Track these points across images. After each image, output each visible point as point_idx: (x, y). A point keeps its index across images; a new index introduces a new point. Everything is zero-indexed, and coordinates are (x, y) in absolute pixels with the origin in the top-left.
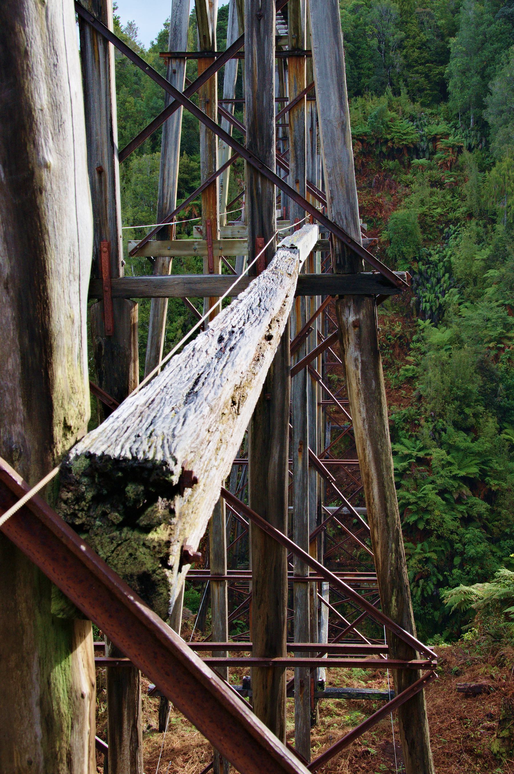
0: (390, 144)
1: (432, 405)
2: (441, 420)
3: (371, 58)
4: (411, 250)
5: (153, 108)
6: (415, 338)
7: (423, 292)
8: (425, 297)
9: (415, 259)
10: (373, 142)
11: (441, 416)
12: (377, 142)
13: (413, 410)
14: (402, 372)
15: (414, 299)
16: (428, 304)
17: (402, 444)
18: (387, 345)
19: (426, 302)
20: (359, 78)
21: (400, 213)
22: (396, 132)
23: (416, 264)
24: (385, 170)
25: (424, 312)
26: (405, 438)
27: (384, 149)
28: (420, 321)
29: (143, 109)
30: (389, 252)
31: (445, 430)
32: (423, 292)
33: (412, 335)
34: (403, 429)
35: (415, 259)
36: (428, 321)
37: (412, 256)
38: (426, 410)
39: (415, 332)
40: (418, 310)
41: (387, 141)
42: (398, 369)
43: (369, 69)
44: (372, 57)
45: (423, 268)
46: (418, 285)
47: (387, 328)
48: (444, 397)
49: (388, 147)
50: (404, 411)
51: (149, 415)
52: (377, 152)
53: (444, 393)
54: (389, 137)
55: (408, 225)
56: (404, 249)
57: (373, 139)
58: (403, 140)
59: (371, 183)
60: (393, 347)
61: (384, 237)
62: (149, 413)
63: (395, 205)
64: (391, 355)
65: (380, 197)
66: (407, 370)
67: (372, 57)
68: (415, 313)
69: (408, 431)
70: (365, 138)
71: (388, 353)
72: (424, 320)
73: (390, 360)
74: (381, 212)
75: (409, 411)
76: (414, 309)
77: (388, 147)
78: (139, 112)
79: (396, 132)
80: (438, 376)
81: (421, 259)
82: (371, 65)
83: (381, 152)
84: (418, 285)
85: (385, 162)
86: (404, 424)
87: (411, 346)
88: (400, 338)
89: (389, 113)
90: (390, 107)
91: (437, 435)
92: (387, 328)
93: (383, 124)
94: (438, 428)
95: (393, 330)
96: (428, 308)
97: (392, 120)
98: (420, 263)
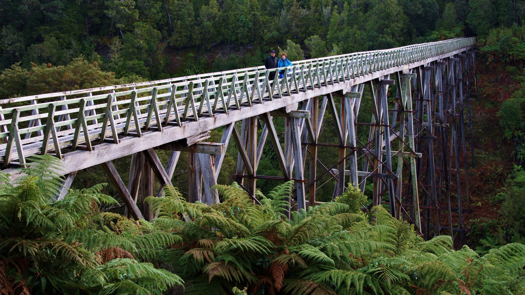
0: (511, 57)
1: (506, 220)
2: (512, 229)
3: (506, 5)
4: (514, 124)
5: (370, 36)
6: (509, 176)
7: (520, 148)
8: (520, 152)
9: (516, 129)
10: (501, 56)
11: (512, 227)
12: (504, 55)
13: (496, 221)
14: (497, 196)
15: (513, 152)
16: (522, 156)
17: (487, 240)
18: (492, 179)
19: (521, 154)
20: (498, 16)
21: (509, 101)
22: (516, 51)
23: (517, 131)
24: (507, 72)
25: (519, 160)
26: (489, 237)
27: (508, 60)
28: (515, 166)
29: (365, 37)
30: (501, 123)
31: (513, 235)
32: (520, 148)
33: (508, 174)
34: (488, 231)
35: (516, 129)
36: (520, 166)
37: (515, 127)
38: (503, 222)
39: (510, 173)
40: (516, 158)
41: (509, 55)
42: (496, 194)
43: (505, 11)
44: (507, 4)
45: (521, 134)
46: (517, 144)
47: (493, 169)
48: (514, 217)
49: (510, 59)
50: (490, 221)
51: (313, 62)
52: (503, 61)
53: (514, 214)
54: (511, 53)
55: (512, 109)
56: (509, 123)
57: (501, 54)
58: (520, 55)
59: (497, 79)
60: (495, 180)
61: (498, 114)
62: (312, 63)
63: (509, 95)
64: (493, 185)
65: (501, 89)
66: (501, 196)
67: (507, 4)
68: (514, 160)
69: (491, 233)
70: (496, 53)
71: (492, 184)
72: (518, 165)
73: (492, 188)
74: (500, 98)
75: (493, 221)
76: (514, 157)
77: (510, 59)
78: (362, 39)
79: (516, 51)
80: (511, 204)
81: (520, 129)
82: (506, 9)
83: (506, 61)
84: (517, 144)
85: (508, 67)
86: (489, 229)
87: (507, 181)
88: (501, 175)
89: (513, 38)
90: (515, 35)
91: (509, 237)
92: (493, 169)
93: (508, 45)
94: (509, 233)
95: (497, 170)
96: (522, 158)
97: (515, 43)
98: (520, 131)
